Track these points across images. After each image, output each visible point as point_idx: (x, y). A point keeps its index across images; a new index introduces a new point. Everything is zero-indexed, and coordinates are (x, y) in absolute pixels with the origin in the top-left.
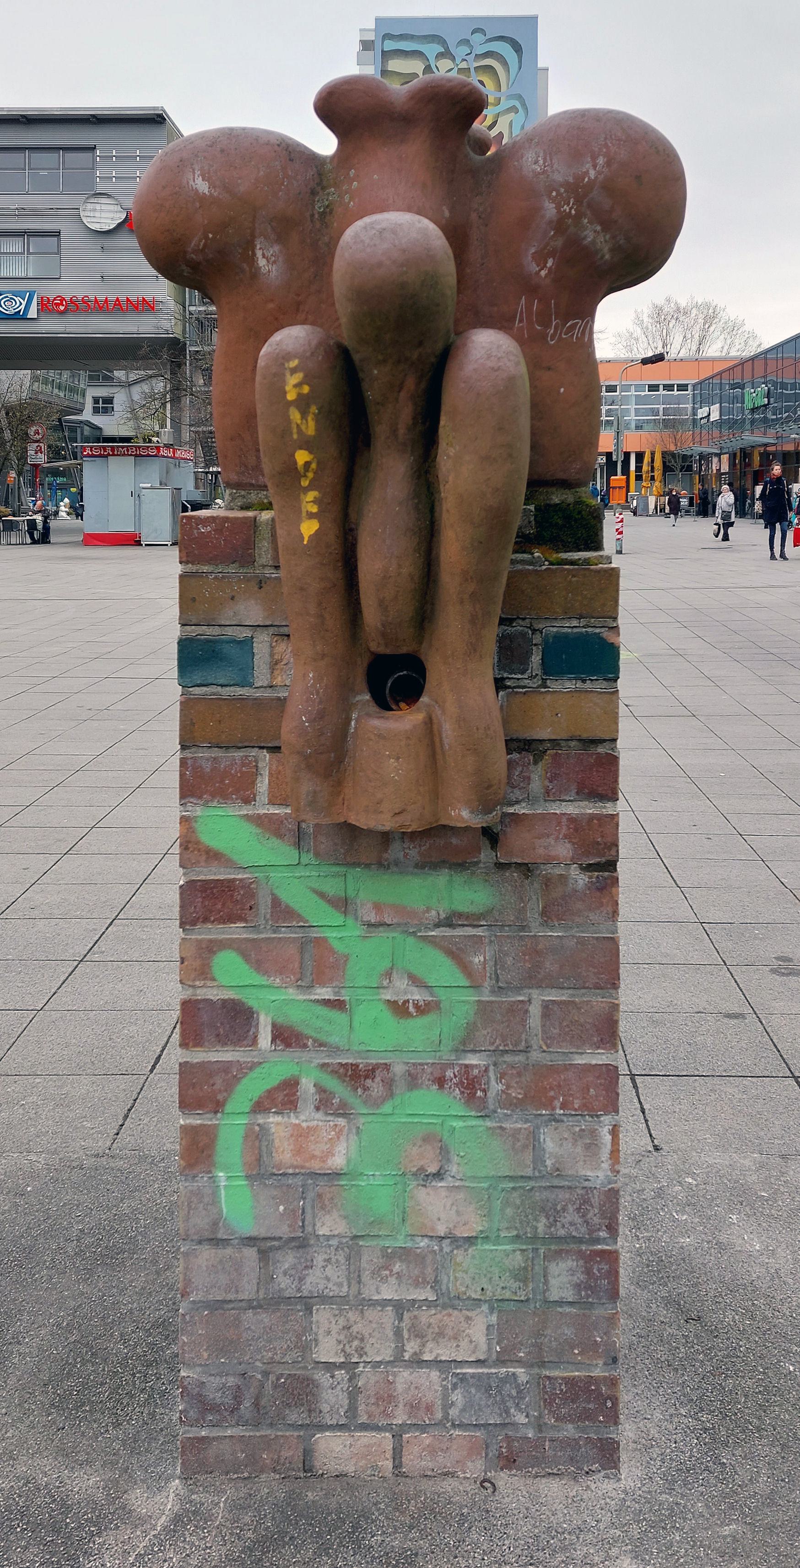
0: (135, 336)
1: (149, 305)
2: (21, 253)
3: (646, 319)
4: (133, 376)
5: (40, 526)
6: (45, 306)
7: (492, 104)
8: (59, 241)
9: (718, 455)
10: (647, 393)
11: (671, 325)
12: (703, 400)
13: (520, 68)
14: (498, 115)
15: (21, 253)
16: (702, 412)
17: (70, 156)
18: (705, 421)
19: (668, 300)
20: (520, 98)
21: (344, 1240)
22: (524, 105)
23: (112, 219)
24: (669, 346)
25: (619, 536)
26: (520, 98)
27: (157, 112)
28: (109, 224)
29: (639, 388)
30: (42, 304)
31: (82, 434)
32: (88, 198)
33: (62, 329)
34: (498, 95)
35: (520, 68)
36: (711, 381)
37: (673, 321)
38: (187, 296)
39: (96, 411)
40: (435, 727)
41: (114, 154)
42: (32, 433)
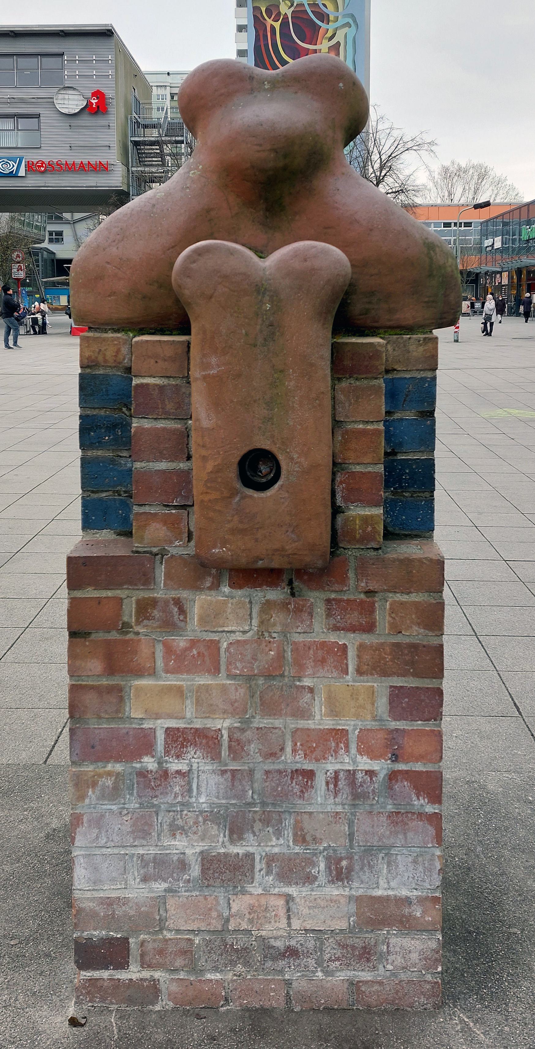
0: (94, 188)
1: (104, 167)
2: (12, 130)
3: (437, 176)
4: (78, 216)
5: (40, 322)
6: (30, 167)
7: (332, 21)
8: (39, 122)
9: (500, 273)
10: (442, 228)
11: (454, 181)
12: (485, 234)
14: (336, 29)
15: (12, 130)
16: (488, 242)
17: (45, 60)
18: (490, 248)
19: (453, 163)
20: (352, 16)
22: (355, 21)
23: (77, 105)
24: (453, 195)
25: (456, 330)
26: (352, 16)
27: (107, 28)
29: (436, 225)
30: (29, 167)
31: (42, 257)
32: (59, 90)
33: (43, 184)
34: (336, 14)
36: (495, 220)
37: (456, 177)
38: (130, 160)
39: (51, 241)
41: (77, 58)
42: (15, 257)
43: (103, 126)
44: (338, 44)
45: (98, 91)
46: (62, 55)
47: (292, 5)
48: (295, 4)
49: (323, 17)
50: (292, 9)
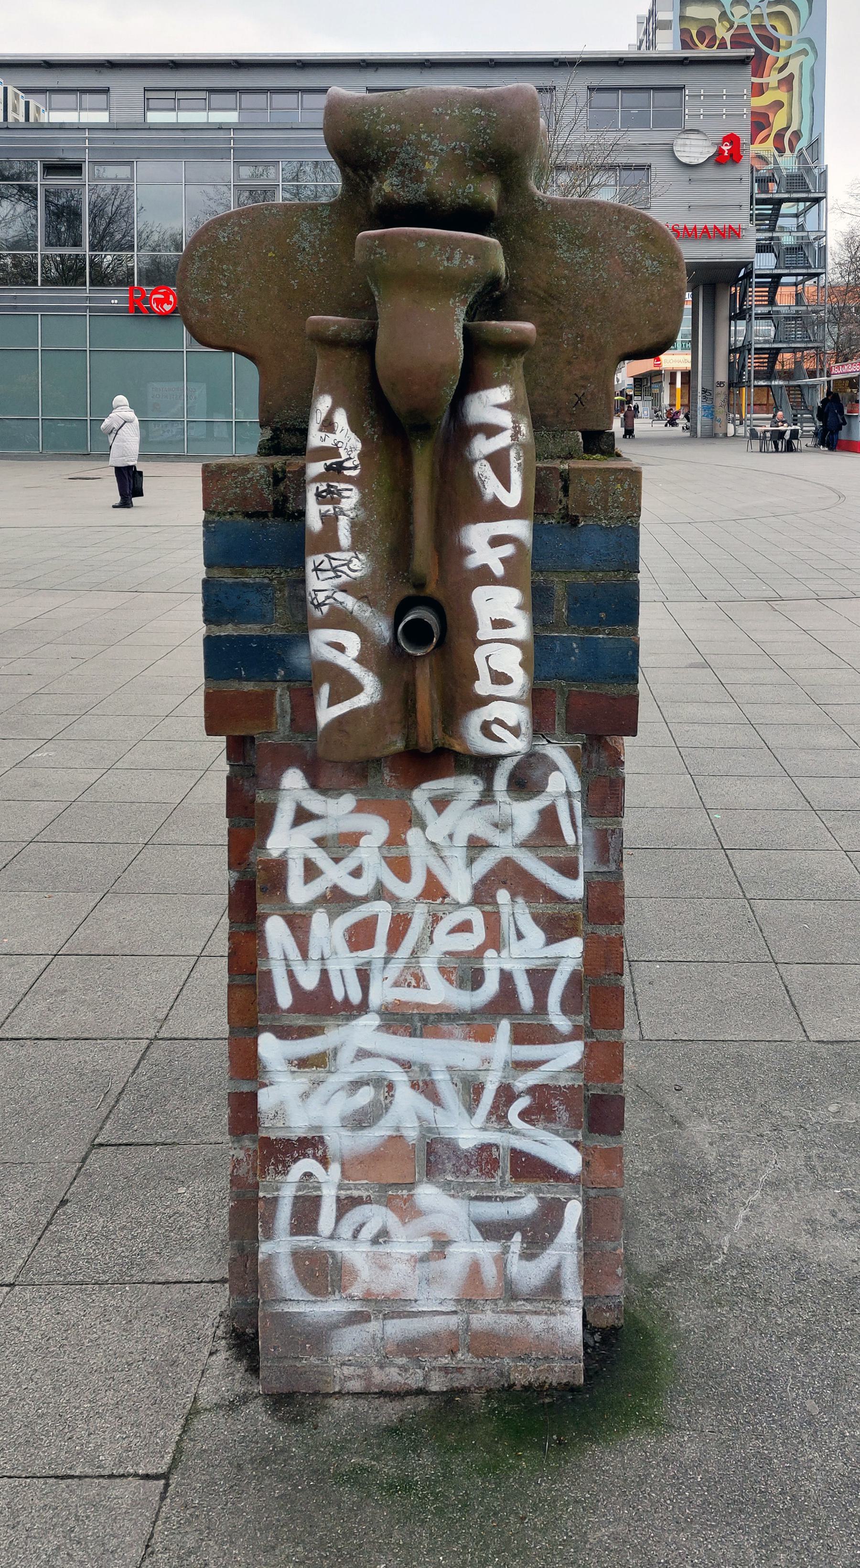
1: (735, 232)
13: (810, 14)
14: (789, 57)
17: (306, 97)
20: (810, 41)
22: (813, 48)
23: (701, 153)
26: (810, 41)
28: (698, 158)
34: (789, 38)
35: (810, 14)
40: (437, 561)
43: (734, 180)
44: (791, 76)
45: (732, 134)
46: (681, 88)
47: (731, 27)
48: (735, 26)
49: (772, 42)
50: (732, 32)
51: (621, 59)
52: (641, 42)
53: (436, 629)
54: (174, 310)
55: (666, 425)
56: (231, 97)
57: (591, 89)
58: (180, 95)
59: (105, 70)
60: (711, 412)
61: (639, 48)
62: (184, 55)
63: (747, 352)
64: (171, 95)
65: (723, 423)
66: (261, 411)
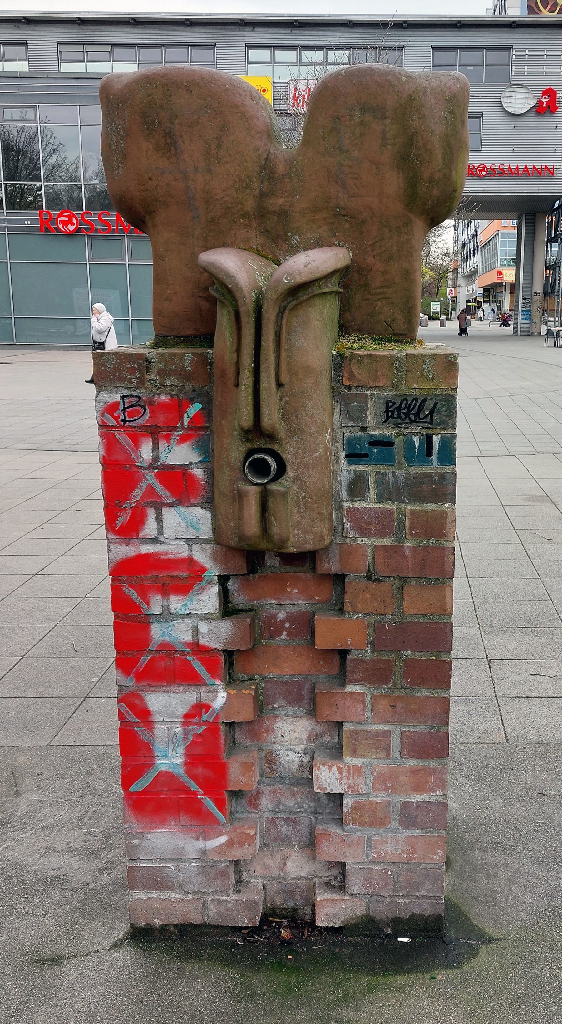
0: (549, 194)
1: (550, 171)
17: (195, 51)
21: (230, 905)
28: (522, 109)
32: (507, 88)
33: (537, 190)
45: (550, 88)
46: (509, 48)
51: (459, 22)
52: (496, 7)
53: (272, 474)
54: (78, 230)
55: (500, 326)
56: (131, 50)
57: (434, 48)
58: (87, 48)
59: (21, 26)
60: (528, 315)
61: (494, 13)
62: (89, 13)
63: (558, 268)
64: (80, 48)
65: (538, 324)
66: (155, 310)
